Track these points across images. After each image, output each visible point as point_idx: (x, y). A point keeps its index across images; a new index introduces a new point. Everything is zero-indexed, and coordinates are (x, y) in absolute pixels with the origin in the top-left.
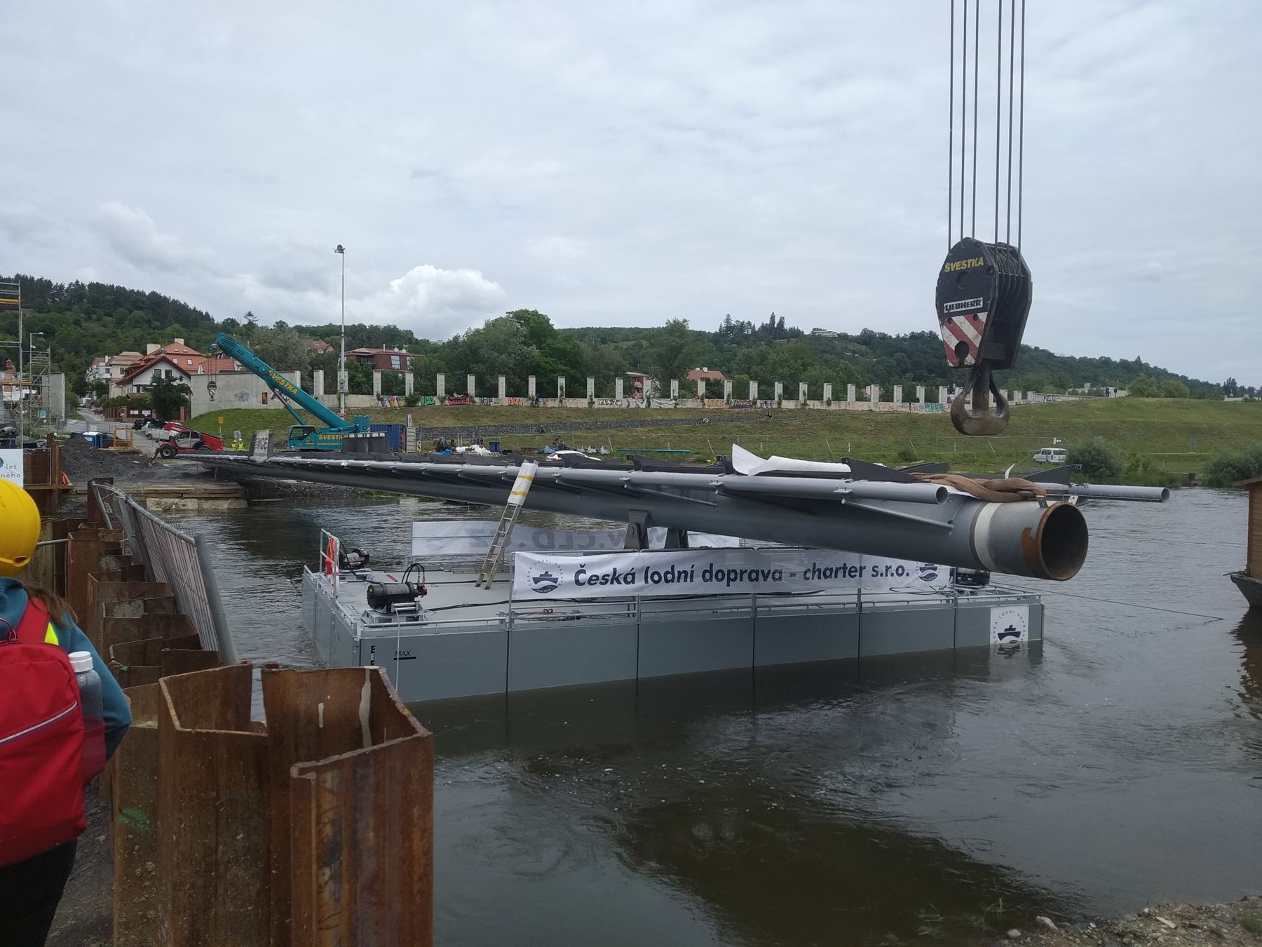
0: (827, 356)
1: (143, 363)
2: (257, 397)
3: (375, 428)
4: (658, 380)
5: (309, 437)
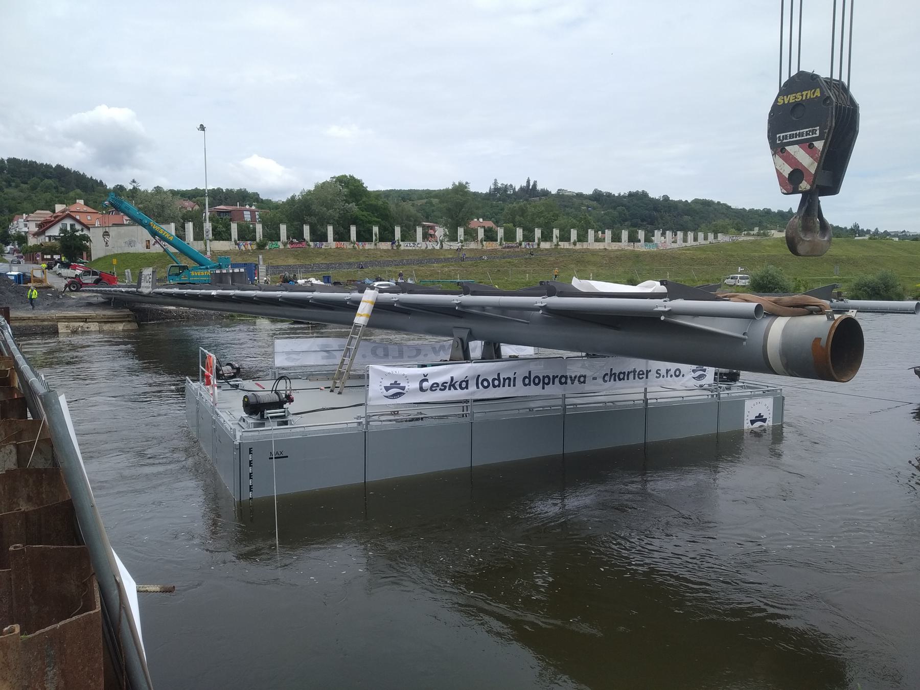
1: (53, 219)
2: (142, 243)
3: (234, 266)
4: (447, 228)
5: (184, 274)
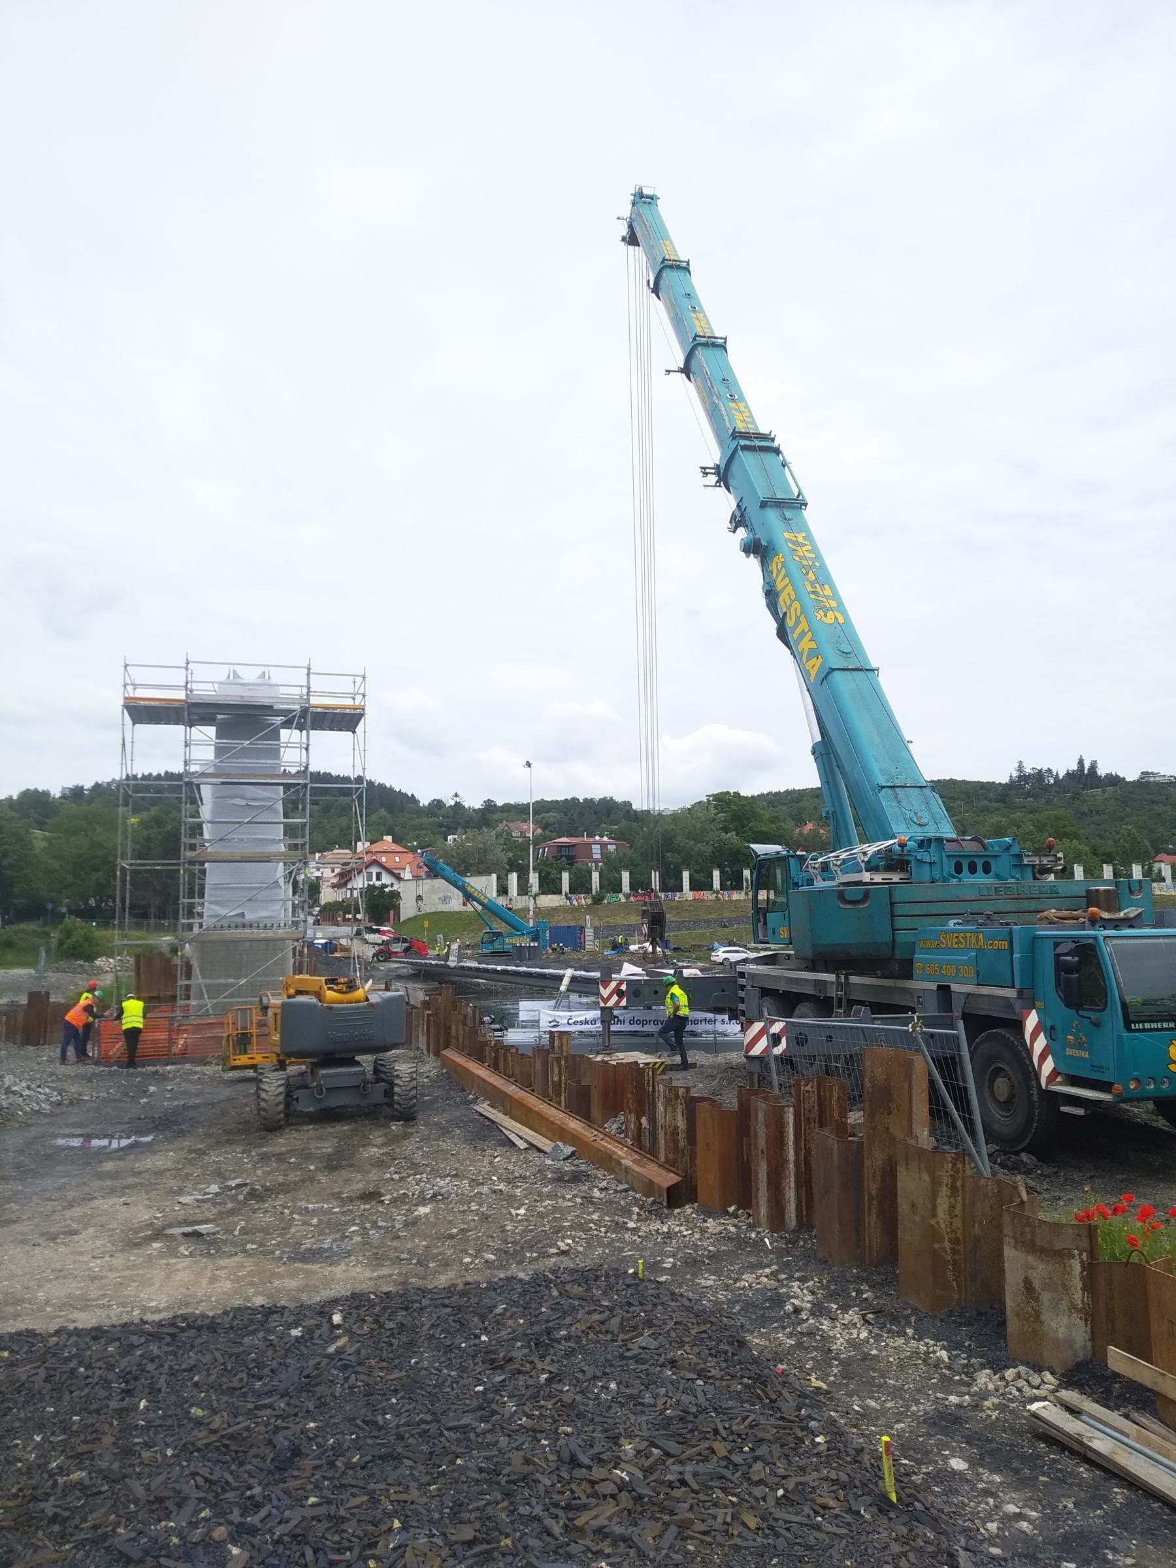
0: (1158, 808)
